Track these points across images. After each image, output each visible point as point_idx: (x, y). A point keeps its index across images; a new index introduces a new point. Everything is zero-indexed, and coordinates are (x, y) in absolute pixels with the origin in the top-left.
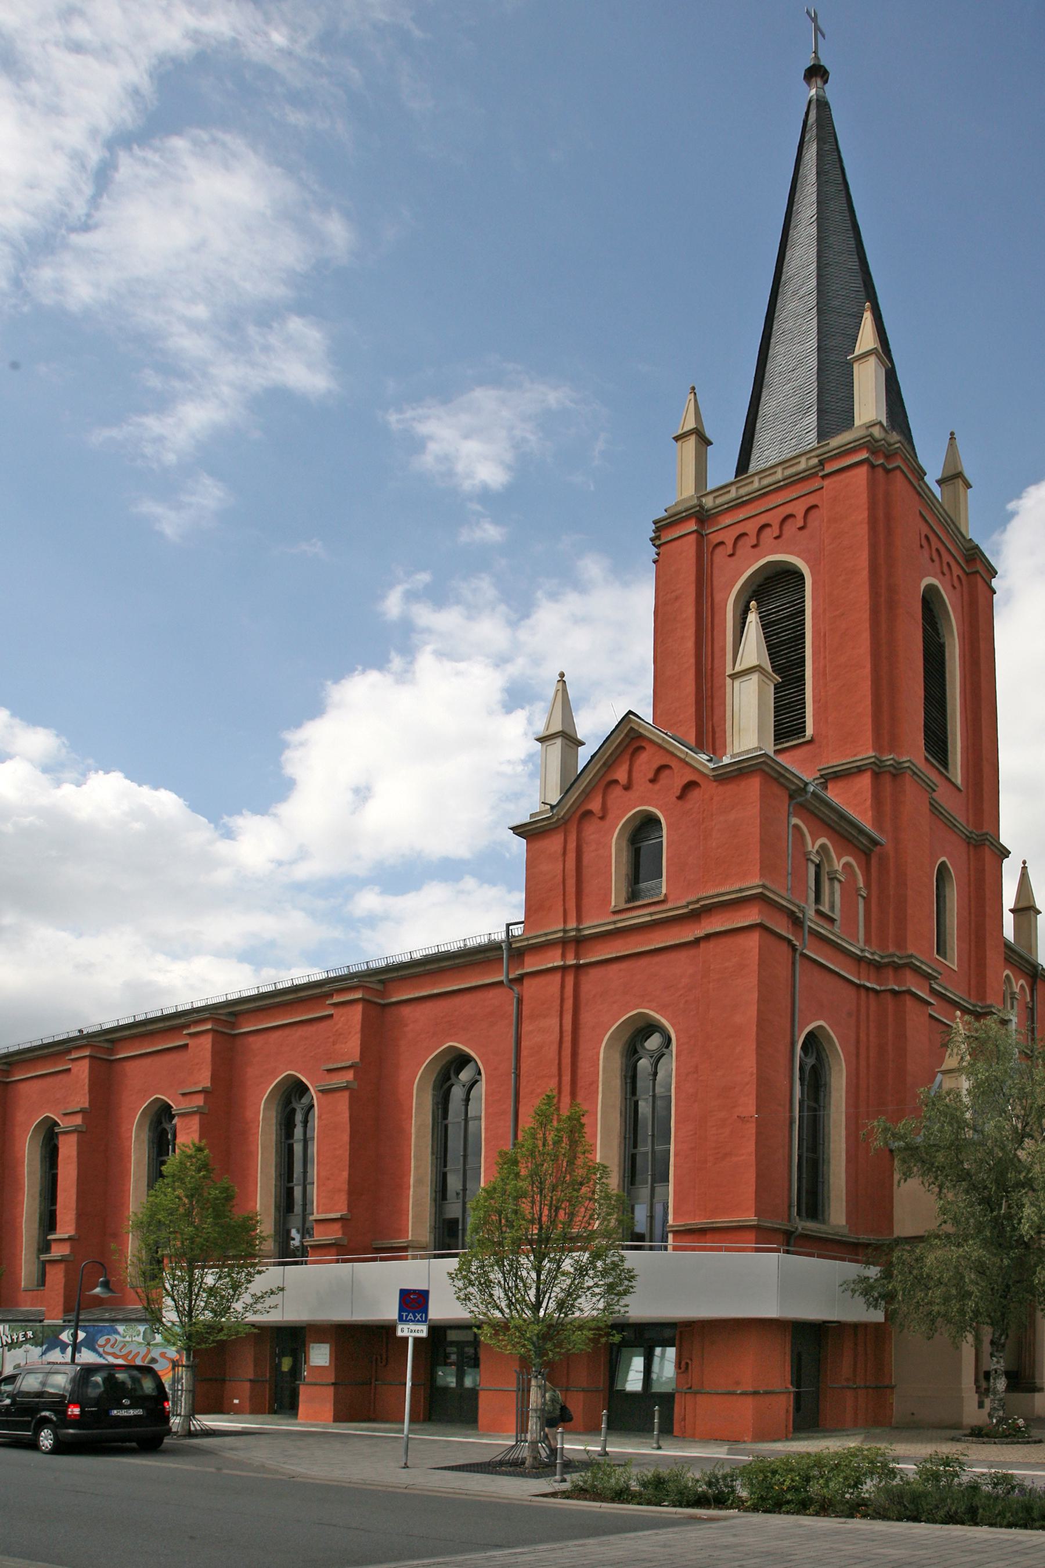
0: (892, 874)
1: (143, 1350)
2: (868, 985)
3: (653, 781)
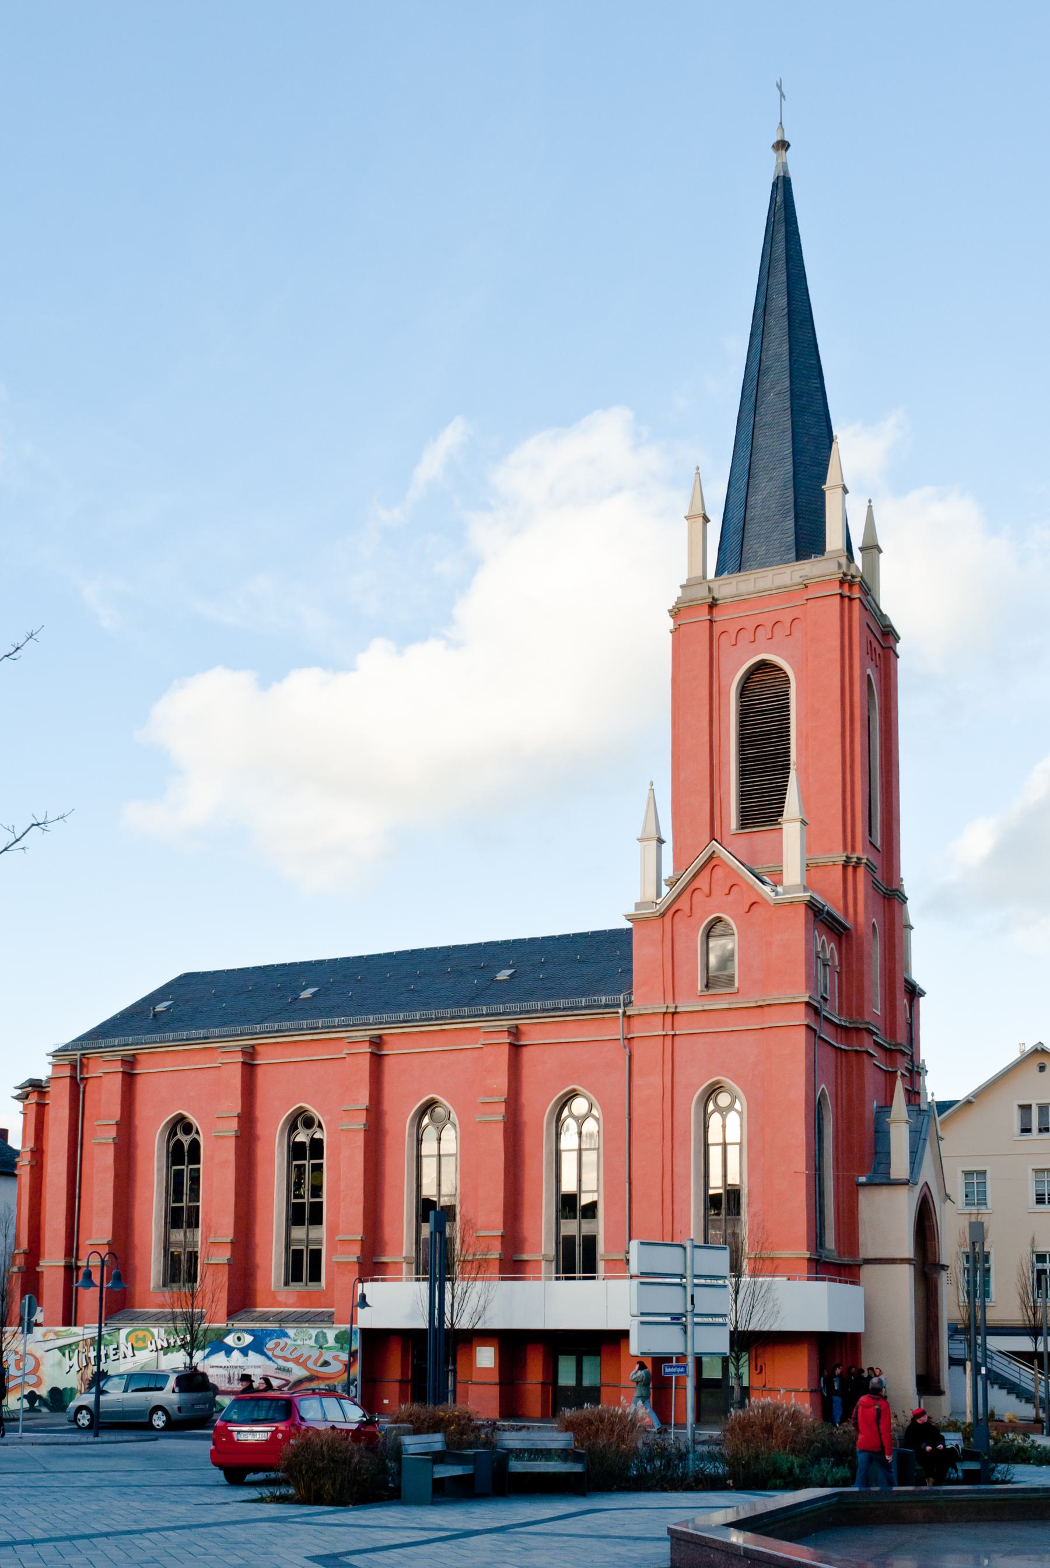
0: (854, 953)
1: (315, 1353)
2: (843, 1047)
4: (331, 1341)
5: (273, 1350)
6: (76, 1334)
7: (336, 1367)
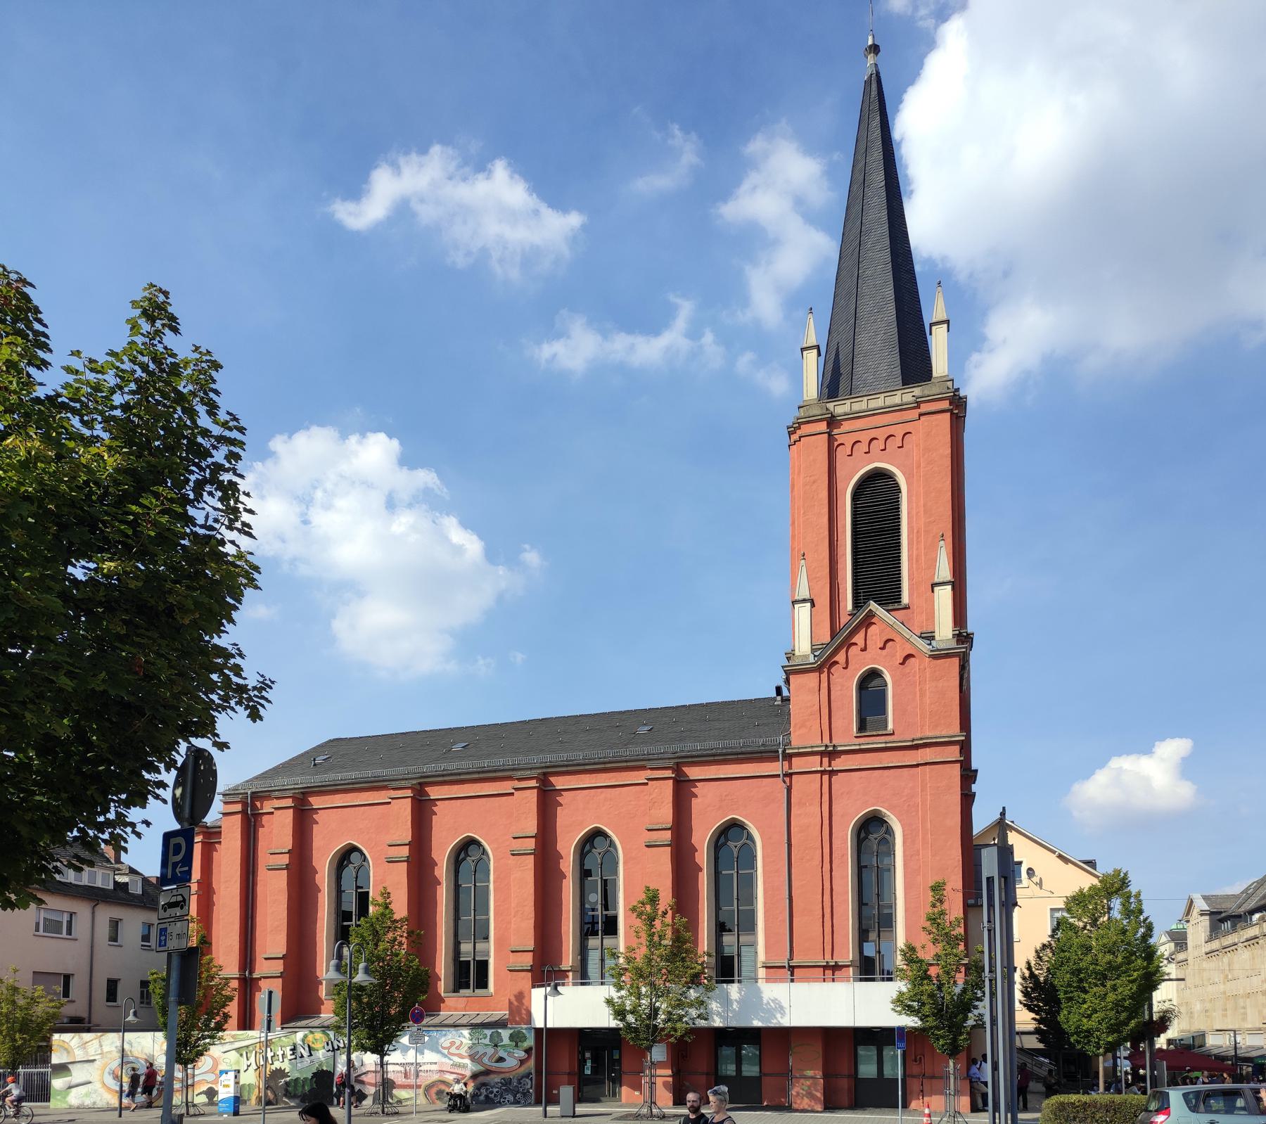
1: (490, 1051)
3: (883, 648)
4: (506, 1041)
5: (448, 1048)
6: (252, 1038)
7: (511, 1063)
